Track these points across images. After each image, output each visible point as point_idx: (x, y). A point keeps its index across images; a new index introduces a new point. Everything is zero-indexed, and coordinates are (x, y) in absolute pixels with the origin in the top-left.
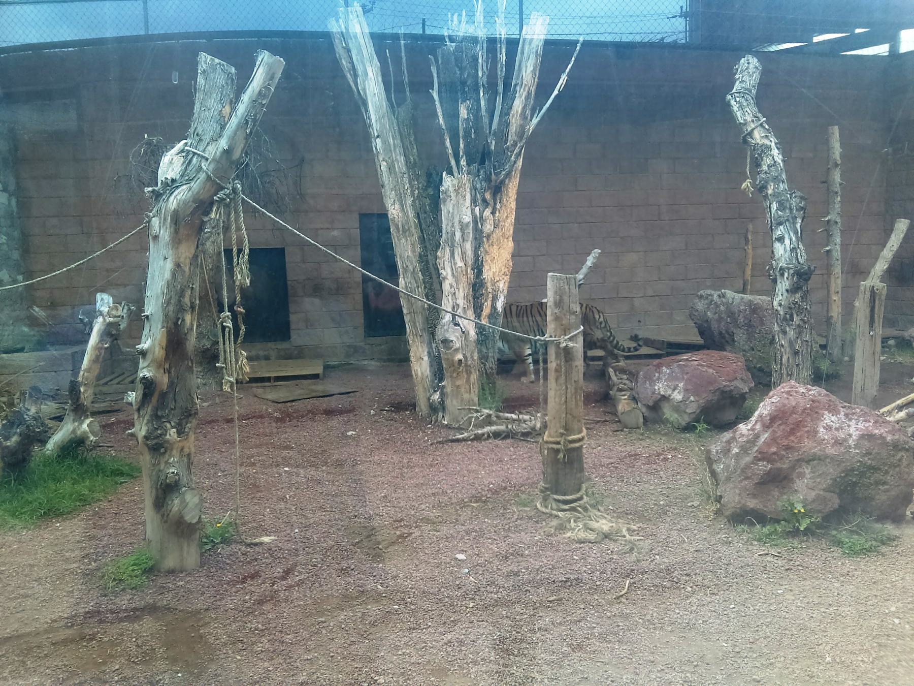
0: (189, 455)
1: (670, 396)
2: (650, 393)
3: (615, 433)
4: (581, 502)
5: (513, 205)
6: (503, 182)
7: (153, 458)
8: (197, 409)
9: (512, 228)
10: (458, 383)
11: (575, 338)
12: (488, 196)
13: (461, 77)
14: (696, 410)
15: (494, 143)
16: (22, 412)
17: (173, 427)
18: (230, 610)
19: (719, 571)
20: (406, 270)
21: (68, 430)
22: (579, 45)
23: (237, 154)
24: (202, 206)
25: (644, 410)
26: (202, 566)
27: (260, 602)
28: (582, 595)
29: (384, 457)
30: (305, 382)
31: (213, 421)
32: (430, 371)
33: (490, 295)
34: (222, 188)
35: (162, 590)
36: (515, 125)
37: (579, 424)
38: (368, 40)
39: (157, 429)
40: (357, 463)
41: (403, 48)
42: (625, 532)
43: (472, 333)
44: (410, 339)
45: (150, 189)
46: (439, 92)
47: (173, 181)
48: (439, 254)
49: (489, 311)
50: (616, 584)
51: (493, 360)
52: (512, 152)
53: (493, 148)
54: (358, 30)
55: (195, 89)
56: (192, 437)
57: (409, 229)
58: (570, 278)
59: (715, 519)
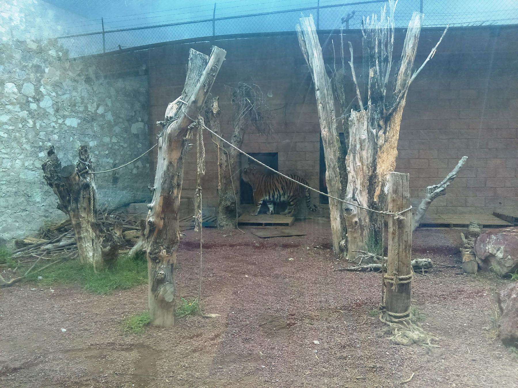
0: (172, 265)
1: (495, 254)
2: (483, 251)
3: (457, 275)
4: (407, 318)
5: (398, 128)
6: (391, 114)
7: (153, 264)
8: (178, 240)
9: (396, 142)
10: (355, 235)
11: (405, 214)
12: (381, 123)
13: (371, 53)
14: (512, 265)
15: (385, 91)
16: (113, 234)
17: (164, 249)
18: (177, 353)
19: (482, 376)
20: (329, 167)
21: (139, 245)
22: (446, 30)
23: (199, 104)
24: (183, 131)
25: (480, 262)
26: (174, 326)
27: (194, 351)
28: (380, 378)
29: (302, 276)
30: (280, 227)
31: (224, 245)
32: (341, 227)
33: (380, 183)
34: (192, 122)
35: (150, 336)
36: (400, 80)
37: (408, 269)
38: (316, 36)
39: (156, 249)
40: (286, 277)
41: (342, 37)
42: (428, 341)
43: (365, 206)
44: (330, 207)
45: (159, 122)
46: (354, 63)
47: (171, 118)
48: (347, 158)
49: (379, 193)
50: (406, 374)
51: (380, 223)
52: (398, 96)
53: (385, 94)
54: (309, 30)
55: (187, 68)
56: (175, 255)
57: (333, 143)
58: (403, 175)
59: (496, 340)
